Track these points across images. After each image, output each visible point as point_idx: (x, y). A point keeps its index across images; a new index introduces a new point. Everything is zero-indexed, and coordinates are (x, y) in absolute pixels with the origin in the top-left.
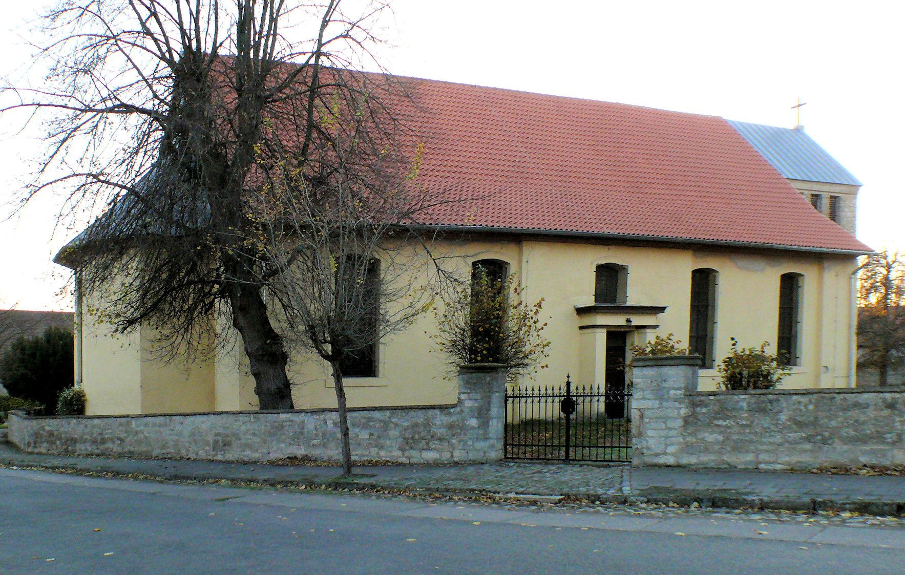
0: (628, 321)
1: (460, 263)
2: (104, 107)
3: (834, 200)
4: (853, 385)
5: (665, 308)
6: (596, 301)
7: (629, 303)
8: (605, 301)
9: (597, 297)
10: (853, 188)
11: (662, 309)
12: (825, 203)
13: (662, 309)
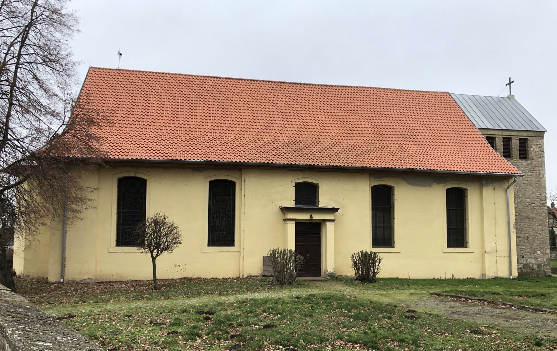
0: (311, 216)
1: (284, 192)
2: (146, 274)
3: (523, 143)
4: (515, 274)
5: (338, 209)
6: (295, 204)
7: (321, 205)
8: (301, 204)
9: (297, 201)
10: (540, 134)
11: (336, 210)
12: (515, 144)
13: (336, 210)
